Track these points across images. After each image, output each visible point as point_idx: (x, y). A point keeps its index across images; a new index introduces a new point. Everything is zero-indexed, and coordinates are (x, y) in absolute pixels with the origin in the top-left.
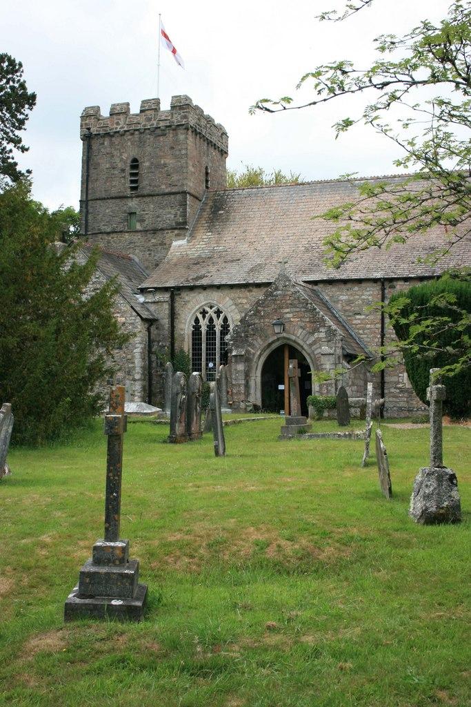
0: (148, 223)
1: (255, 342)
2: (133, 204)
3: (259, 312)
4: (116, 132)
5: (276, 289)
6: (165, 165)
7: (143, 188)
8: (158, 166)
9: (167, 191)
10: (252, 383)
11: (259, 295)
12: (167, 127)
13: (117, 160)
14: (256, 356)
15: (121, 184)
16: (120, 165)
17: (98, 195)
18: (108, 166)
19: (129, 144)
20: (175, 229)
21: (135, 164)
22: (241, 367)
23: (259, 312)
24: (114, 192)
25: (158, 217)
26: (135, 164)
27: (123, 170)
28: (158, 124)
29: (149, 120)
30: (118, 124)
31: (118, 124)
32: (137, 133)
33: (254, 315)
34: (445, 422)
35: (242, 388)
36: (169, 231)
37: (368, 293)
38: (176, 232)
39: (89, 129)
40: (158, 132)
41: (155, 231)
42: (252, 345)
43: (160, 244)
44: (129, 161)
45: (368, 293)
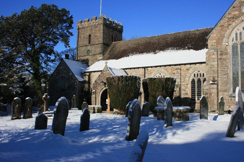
0: (93, 53)
1: (98, 88)
2: (89, 48)
3: (99, 79)
4: (85, 27)
5: (104, 72)
6: (97, 36)
7: (92, 43)
8: (96, 36)
9: (97, 43)
10: (97, 101)
11: (100, 73)
12: (98, 24)
13: (85, 35)
14: (99, 92)
15: (86, 42)
16: (86, 37)
17: (81, 46)
18: (83, 37)
19: (88, 30)
20: (99, 54)
21: (90, 36)
22: (94, 96)
23: (99, 79)
24: (84, 45)
25: (95, 51)
26: (90, 36)
27: (87, 38)
28: (95, 24)
29: (93, 23)
30: (86, 25)
31: (86, 25)
32: (90, 27)
33: (98, 79)
34: (35, 118)
35: (95, 102)
36: (98, 55)
37: (141, 72)
38: (100, 55)
39: (79, 27)
40: (95, 26)
41: (94, 55)
42: (97, 89)
43: (96, 59)
44: (88, 35)
45: (141, 72)
